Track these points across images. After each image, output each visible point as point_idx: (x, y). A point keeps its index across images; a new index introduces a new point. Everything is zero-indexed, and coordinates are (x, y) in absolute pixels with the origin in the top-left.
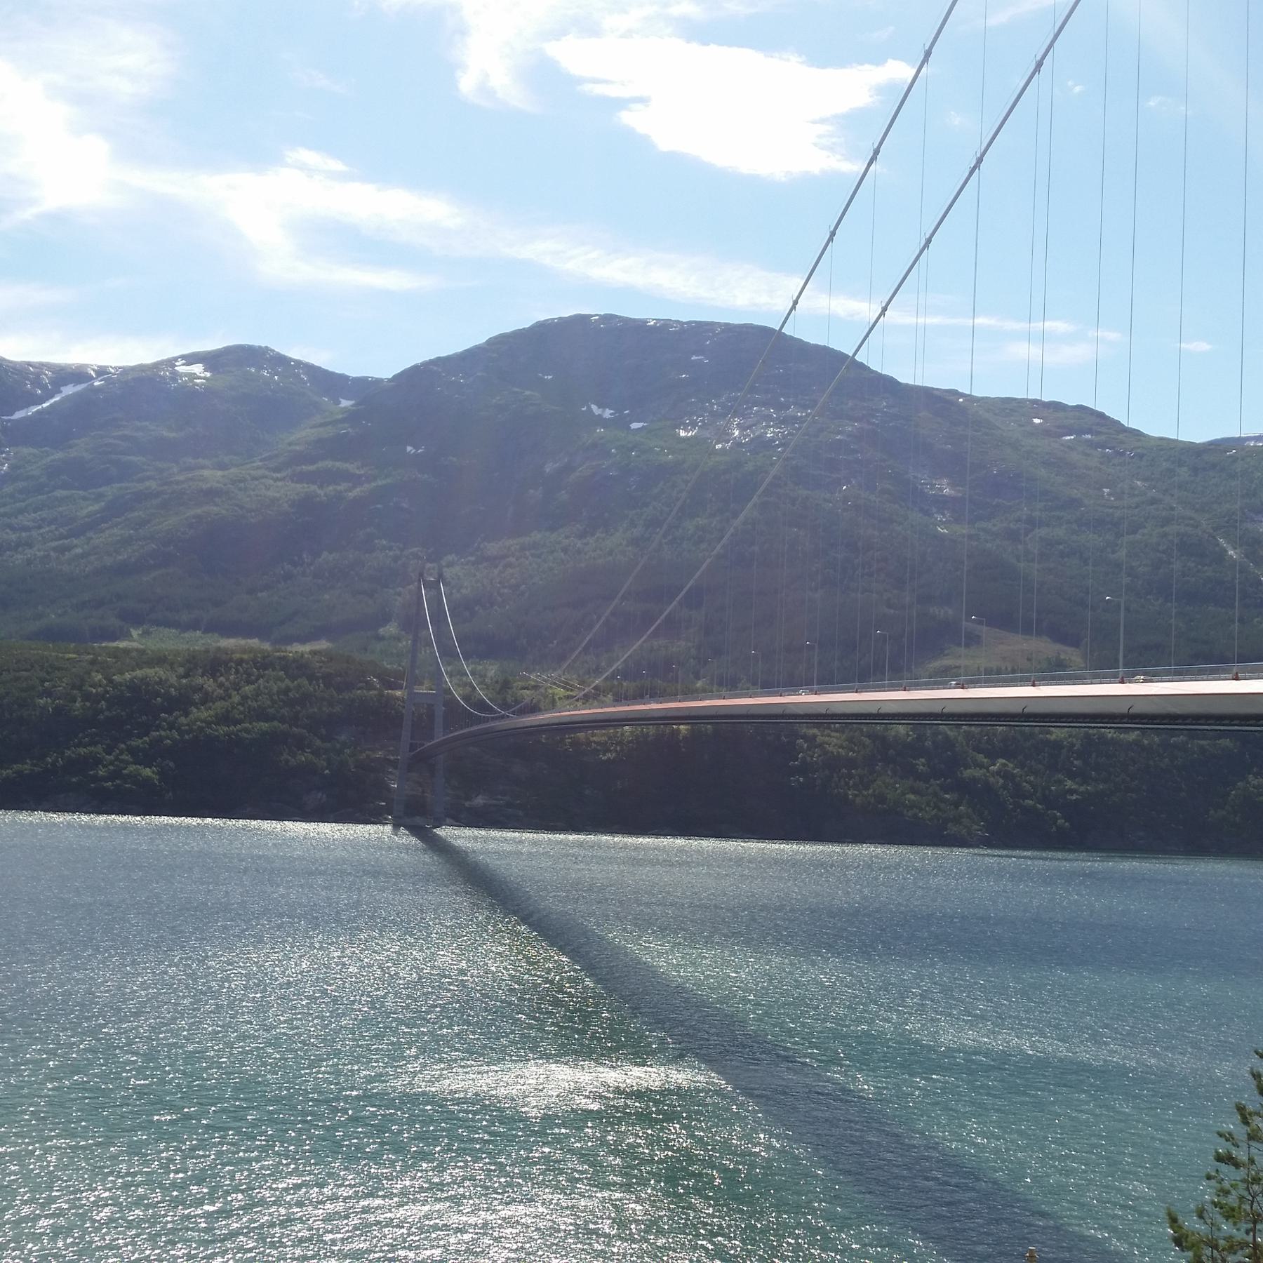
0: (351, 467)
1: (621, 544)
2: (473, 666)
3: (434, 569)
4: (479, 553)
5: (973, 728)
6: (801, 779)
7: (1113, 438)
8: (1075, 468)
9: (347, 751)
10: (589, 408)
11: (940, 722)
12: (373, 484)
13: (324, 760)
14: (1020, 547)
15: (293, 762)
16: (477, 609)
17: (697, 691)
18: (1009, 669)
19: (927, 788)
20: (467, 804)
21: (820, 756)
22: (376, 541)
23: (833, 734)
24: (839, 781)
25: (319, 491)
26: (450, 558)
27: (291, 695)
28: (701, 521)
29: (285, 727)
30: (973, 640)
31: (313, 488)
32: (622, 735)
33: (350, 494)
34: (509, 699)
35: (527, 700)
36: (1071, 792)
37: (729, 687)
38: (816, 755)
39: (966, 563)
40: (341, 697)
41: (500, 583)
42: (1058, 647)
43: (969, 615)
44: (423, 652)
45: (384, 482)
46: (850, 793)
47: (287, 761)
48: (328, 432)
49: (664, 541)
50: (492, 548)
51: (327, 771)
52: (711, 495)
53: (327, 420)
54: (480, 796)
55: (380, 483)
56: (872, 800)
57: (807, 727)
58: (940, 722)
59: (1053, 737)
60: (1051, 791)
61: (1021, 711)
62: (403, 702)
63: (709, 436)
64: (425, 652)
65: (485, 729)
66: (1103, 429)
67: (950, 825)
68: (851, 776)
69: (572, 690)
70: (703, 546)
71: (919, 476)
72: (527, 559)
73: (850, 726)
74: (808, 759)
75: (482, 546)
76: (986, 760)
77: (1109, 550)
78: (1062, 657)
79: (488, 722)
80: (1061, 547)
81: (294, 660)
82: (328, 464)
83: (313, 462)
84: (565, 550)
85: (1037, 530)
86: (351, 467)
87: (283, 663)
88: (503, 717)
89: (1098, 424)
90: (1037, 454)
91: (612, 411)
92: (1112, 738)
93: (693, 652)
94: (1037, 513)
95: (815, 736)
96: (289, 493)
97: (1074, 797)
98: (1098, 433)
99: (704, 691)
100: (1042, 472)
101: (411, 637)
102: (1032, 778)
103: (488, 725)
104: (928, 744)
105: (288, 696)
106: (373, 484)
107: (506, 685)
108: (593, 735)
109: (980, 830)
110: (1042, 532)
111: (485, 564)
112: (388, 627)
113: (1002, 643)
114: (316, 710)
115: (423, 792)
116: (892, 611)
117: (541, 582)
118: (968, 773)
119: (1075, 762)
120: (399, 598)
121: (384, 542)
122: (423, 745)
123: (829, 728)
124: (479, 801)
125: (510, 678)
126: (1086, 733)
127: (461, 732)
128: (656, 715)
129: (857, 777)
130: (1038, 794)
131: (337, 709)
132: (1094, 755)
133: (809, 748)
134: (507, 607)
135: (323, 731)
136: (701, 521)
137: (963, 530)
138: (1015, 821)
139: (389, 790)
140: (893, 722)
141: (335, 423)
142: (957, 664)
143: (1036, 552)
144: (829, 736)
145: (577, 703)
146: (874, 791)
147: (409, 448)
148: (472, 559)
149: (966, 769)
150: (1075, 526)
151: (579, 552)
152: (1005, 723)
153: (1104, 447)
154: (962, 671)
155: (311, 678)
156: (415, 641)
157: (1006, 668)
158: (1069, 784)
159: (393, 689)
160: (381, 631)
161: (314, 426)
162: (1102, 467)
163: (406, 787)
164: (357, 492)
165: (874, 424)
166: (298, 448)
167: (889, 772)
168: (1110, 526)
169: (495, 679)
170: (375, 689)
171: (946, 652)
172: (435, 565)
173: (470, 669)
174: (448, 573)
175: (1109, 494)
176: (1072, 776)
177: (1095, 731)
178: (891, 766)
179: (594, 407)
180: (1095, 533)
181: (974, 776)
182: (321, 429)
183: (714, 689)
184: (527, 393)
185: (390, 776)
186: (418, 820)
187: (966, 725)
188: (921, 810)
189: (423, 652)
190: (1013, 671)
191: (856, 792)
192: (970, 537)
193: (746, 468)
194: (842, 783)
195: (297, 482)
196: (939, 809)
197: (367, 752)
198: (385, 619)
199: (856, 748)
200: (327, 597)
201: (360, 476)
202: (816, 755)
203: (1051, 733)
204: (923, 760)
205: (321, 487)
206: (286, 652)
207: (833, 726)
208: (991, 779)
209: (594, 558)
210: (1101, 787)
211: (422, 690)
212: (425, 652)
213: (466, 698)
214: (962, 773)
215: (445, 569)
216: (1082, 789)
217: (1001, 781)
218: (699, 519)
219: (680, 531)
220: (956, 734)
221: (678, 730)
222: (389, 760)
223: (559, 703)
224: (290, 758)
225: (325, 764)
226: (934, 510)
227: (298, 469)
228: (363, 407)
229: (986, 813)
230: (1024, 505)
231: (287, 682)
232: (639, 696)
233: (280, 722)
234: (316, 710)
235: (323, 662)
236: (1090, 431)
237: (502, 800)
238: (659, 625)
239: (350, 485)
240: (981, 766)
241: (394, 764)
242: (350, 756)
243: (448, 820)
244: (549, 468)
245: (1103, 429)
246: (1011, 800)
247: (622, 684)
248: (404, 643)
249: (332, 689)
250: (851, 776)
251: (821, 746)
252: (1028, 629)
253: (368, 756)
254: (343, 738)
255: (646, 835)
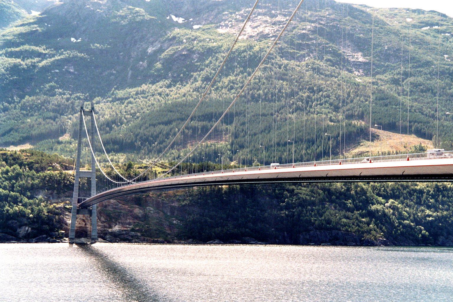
0: (41, 49)
1: (190, 91)
2: (112, 157)
3: (89, 105)
4: (114, 96)
5: (376, 184)
6: (287, 212)
7: (450, 28)
8: (429, 45)
9: (43, 204)
10: (170, 17)
11: (359, 181)
12: (53, 59)
13: (29, 209)
14: (399, 88)
15: (11, 211)
16: (113, 126)
17: (231, 167)
18: (395, 152)
19: (353, 216)
20: (110, 230)
21: (296, 200)
22: (56, 90)
23: (303, 188)
24: (307, 213)
25: (22, 63)
26: (97, 99)
27: (9, 174)
28: (232, 78)
29: (6, 192)
30: (375, 137)
31: (18, 60)
32: (192, 191)
33: (40, 64)
34: (132, 174)
35: (142, 174)
36: (429, 216)
37: (248, 165)
38: (294, 199)
39: (371, 97)
40: (38, 175)
41: (125, 112)
42: (421, 140)
43: (373, 124)
44: (84, 150)
45: (59, 58)
46: (312, 219)
47: (8, 211)
48: (23, 30)
49: (212, 89)
50: (121, 93)
51: (31, 215)
52: (236, 64)
53: (25, 22)
54: (117, 226)
55: (57, 58)
56: (324, 222)
57: (290, 185)
58: (359, 181)
59: (418, 188)
60: (418, 216)
61: (401, 174)
62: (74, 177)
63: (235, 32)
64: (85, 150)
65: (108, 192)
66: (445, 23)
67: (365, 234)
68: (312, 210)
69: (165, 168)
70: (233, 91)
71: (346, 51)
72: (140, 99)
73: (312, 184)
74: (290, 201)
75: (115, 92)
76: (383, 200)
77: (447, 88)
78: (423, 145)
79: (120, 186)
80: (422, 87)
81: (11, 155)
82: (27, 47)
83: (18, 45)
84: (160, 94)
85: (409, 79)
86: (41, 49)
87: (5, 157)
88: (129, 183)
89: (442, 20)
90: (409, 38)
91: (184, 19)
92: (450, 187)
93: (229, 146)
94: (409, 69)
95: (293, 190)
96: (4, 63)
97: (431, 219)
98: (442, 25)
99: (235, 167)
100: (411, 48)
101: (77, 142)
102: (408, 209)
103: (120, 188)
104: (353, 192)
105: (8, 174)
106: (53, 59)
107: (130, 166)
108: (177, 192)
109: (381, 237)
110: (411, 79)
111: (117, 102)
112: (64, 136)
113: (391, 139)
114: (24, 182)
115: (86, 224)
116: (333, 123)
117: (148, 112)
118: (374, 207)
119: (431, 200)
120: (69, 121)
121: (61, 91)
122: (85, 199)
123: (301, 185)
124: (116, 228)
125: (132, 163)
126: (437, 185)
127: (106, 192)
128: (210, 180)
129: (316, 211)
130: (411, 218)
131: (37, 181)
132: (441, 197)
133: (291, 196)
134: (130, 125)
135: (29, 194)
136: (232, 78)
137: (369, 79)
138: (399, 232)
139: (66, 224)
140: (334, 181)
141: (29, 24)
142: (367, 151)
143: (408, 90)
144: (300, 189)
145: (168, 175)
146: (325, 218)
147: (73, 39)
148: (111, 99)
149: (373, 205)
150: (429, 76)
151: (167, 95)
152: (393, 180)
153: (444, 32)
154: (370, 154)
155: (21, 165)
156: (80, 144)
157: (393, 152)
158: (428, 212)
159: (67, 170)
160: (60, 139)
161: (16, 26)
162: (443, 43)
163: (76, 222)
164: (44, 63)
165: (321, 24)
166: (8, 38)
167: (333, 208)
168: (448, 75)
169: (124, 164)
170: (58, 170)
171: (361, 144)
172: (89, 103)
173: (110, 158)
174: (97, 107)
175: (448, 58)
176: (429, 207)
177: (441, 183)
178: (334, 204)
179: (173, 17)
180: (439, 79)
181: (377, 209)
182: (21, 28)
183: (240, 166)
184: (137, 9)
185: (67, 217)
186: (83, 240)
187: (372, 182)
188: (350, 227)
189: (84, 150)
190: (397, 153)
191: (315, 218)
192: (373, 83)
193: (255, 49)
194: (308, 214)
195: (9, 57)
196: (359, 226)
197: (54, 204)
198: (63, 132)
199: (315, 195)
200: (29, 120)
201: (45, 54)
202: (294, 199)
203: (417, 185)
204: (350, 201)
205: (23, 60)
206: (6, 151)
207: (302, 184)
208: (386, 211)
209: (176, 99)
210: (445, 213)
211: (84, 169)
212: (85, 150)
213: (109, 174)
214: (370, 207)
215: (95, 105)
216: (435, 214)
217: (391, 211)
218: (231, 77)
219: (221, 83)
220: (368, 187)
221: (222, 188)
222: (66, 208)
223: (159, 175)
224: (9, 208)
225: (30, 211)
226: (354, 69)
227: (9, 50)
228: (45, 15)
229: (384, 228)
230: (401, 65)
231: (7, 167)
232: (201, 170)
233: (3, 189)
234: (24, 182)
235: (28, 156)
236: (437, 24)
237: (129, 227)
238: (211, 133)
239: (40, 59)
240: (381, 203)
241: (69, 210)
242: (44, 207)
243: (100, 239)
244: (150, 50)
245: (445, 23)
246: (397, 221)
247: (192, 165)
248: (74, 145)
249: (33, 171)
250: (312, 210)
251: (297, 194)
252: (405, 131)
253: (54, 206)
254: (40, 197)
255: (206, 243)
